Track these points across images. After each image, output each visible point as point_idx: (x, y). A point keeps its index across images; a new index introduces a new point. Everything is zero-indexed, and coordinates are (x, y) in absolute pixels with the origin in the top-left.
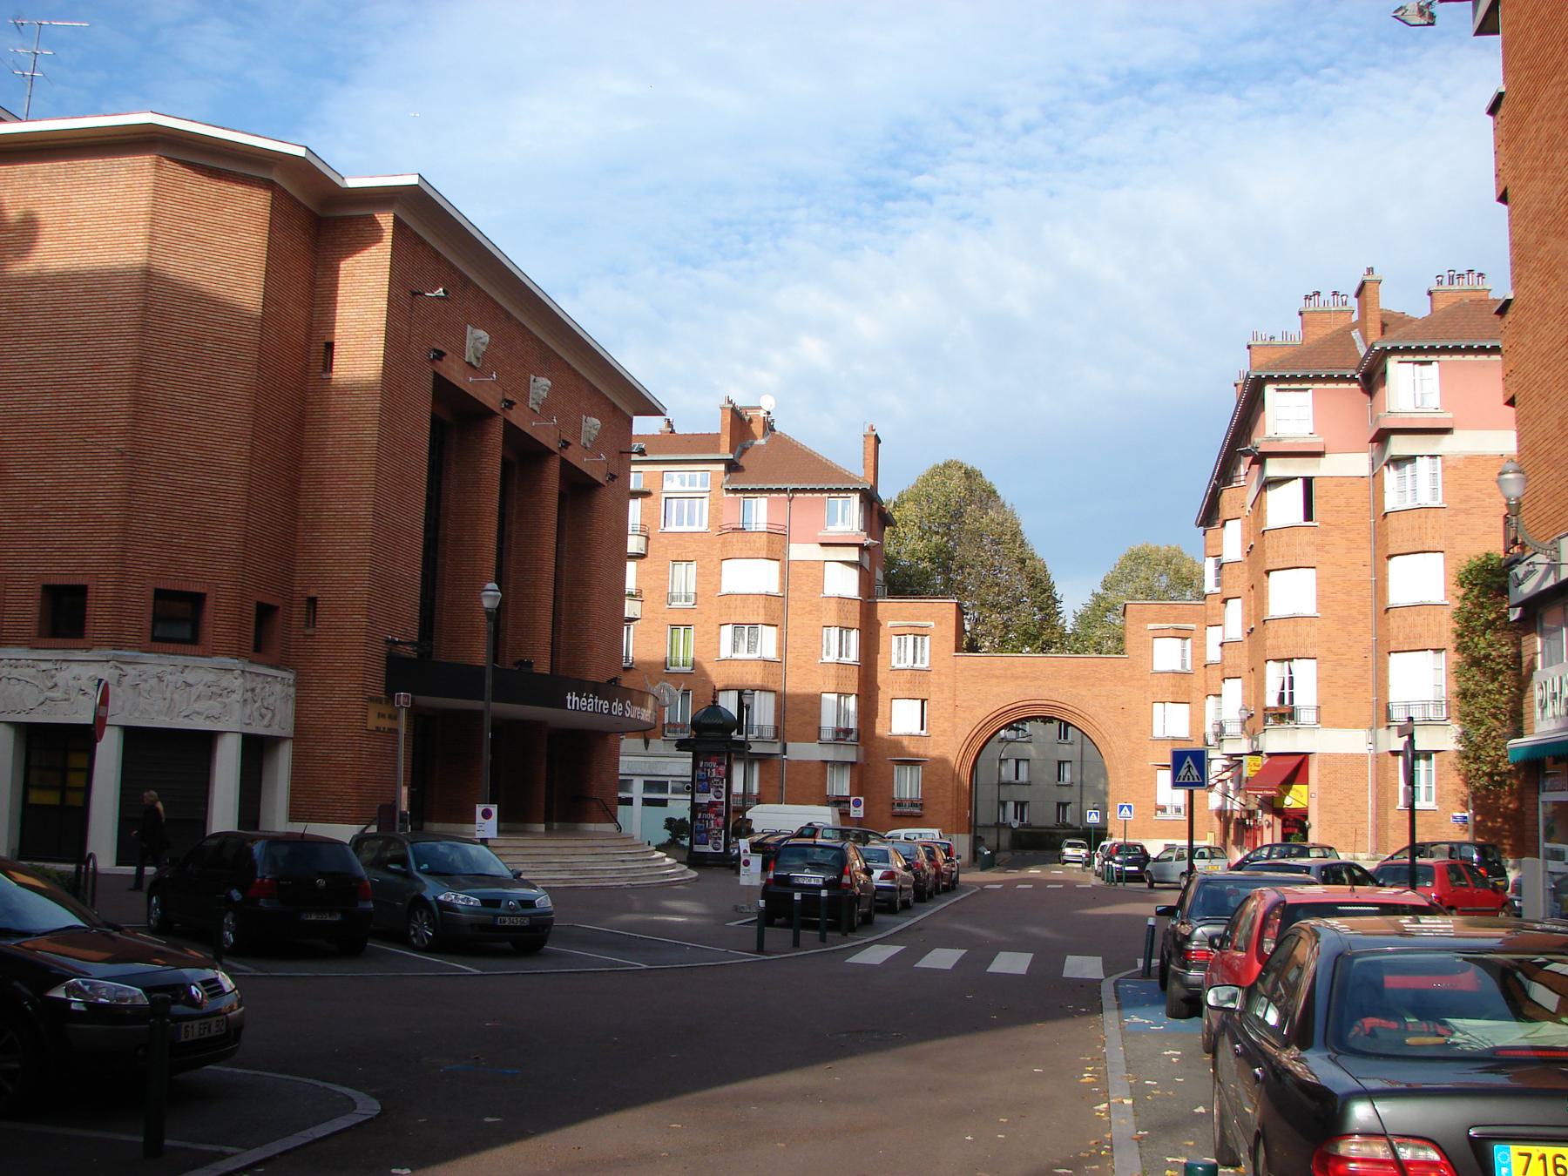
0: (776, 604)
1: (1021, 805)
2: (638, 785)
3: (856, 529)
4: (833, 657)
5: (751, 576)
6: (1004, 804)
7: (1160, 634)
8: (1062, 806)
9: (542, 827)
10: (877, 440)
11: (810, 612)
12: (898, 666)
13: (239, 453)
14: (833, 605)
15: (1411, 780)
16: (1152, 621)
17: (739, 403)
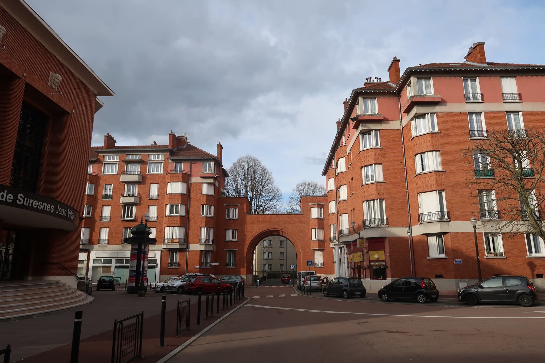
1: (270, 265)
3: (213, 172)
4: (205, 214)
6: (265, 265)
8: (282, 265)
9: (382, 267)
11: (197, 200)
14: (205, 197)
16: (310, 202)
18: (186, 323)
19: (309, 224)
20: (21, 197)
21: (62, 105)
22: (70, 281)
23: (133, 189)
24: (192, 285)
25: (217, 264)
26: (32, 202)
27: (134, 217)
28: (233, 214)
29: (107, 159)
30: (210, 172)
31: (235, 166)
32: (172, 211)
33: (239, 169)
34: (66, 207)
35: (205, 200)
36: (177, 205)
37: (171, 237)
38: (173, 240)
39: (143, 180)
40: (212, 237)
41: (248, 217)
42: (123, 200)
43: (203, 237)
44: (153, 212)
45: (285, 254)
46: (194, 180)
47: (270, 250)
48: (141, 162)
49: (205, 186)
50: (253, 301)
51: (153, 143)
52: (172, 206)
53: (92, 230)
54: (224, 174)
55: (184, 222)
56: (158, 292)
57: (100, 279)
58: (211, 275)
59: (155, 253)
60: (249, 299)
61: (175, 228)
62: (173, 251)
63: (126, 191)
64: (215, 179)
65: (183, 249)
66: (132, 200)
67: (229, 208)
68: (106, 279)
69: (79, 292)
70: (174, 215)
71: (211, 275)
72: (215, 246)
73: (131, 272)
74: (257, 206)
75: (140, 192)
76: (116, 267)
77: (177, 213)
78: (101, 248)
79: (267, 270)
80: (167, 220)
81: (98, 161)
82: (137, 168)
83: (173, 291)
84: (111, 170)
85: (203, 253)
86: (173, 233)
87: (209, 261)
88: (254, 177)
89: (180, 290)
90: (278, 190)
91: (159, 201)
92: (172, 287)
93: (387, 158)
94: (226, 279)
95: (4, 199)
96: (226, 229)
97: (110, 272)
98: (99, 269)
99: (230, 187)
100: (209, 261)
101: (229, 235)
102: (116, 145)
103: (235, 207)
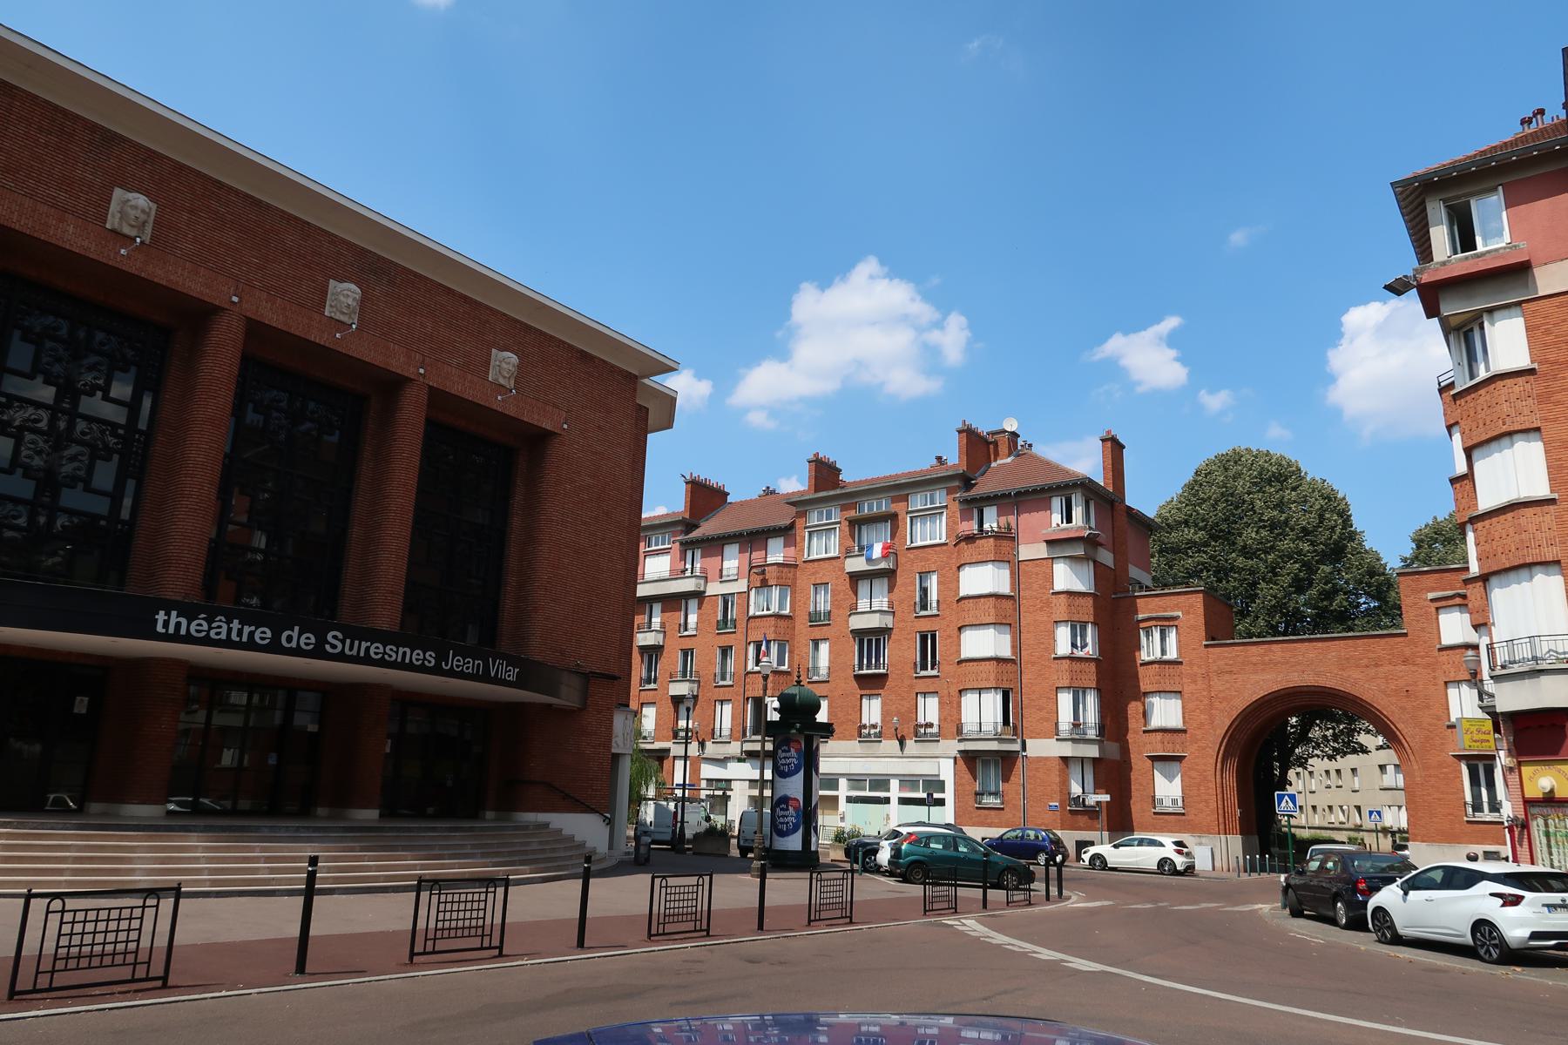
0: (1008, 604)
2: (843, 790)
3: (1080, 524)
5: (982, 579)
7: (1443, 604)
11: (1041, 609)
12: (1147, 659)
15: (1163, 639)
16: (1433, 590)
20: (335, 637)
26: (368, 649)
42: (857, 622)
51: (935, 462)
76: (850, 800)
93: (1558, 403)
95: (294, 644)
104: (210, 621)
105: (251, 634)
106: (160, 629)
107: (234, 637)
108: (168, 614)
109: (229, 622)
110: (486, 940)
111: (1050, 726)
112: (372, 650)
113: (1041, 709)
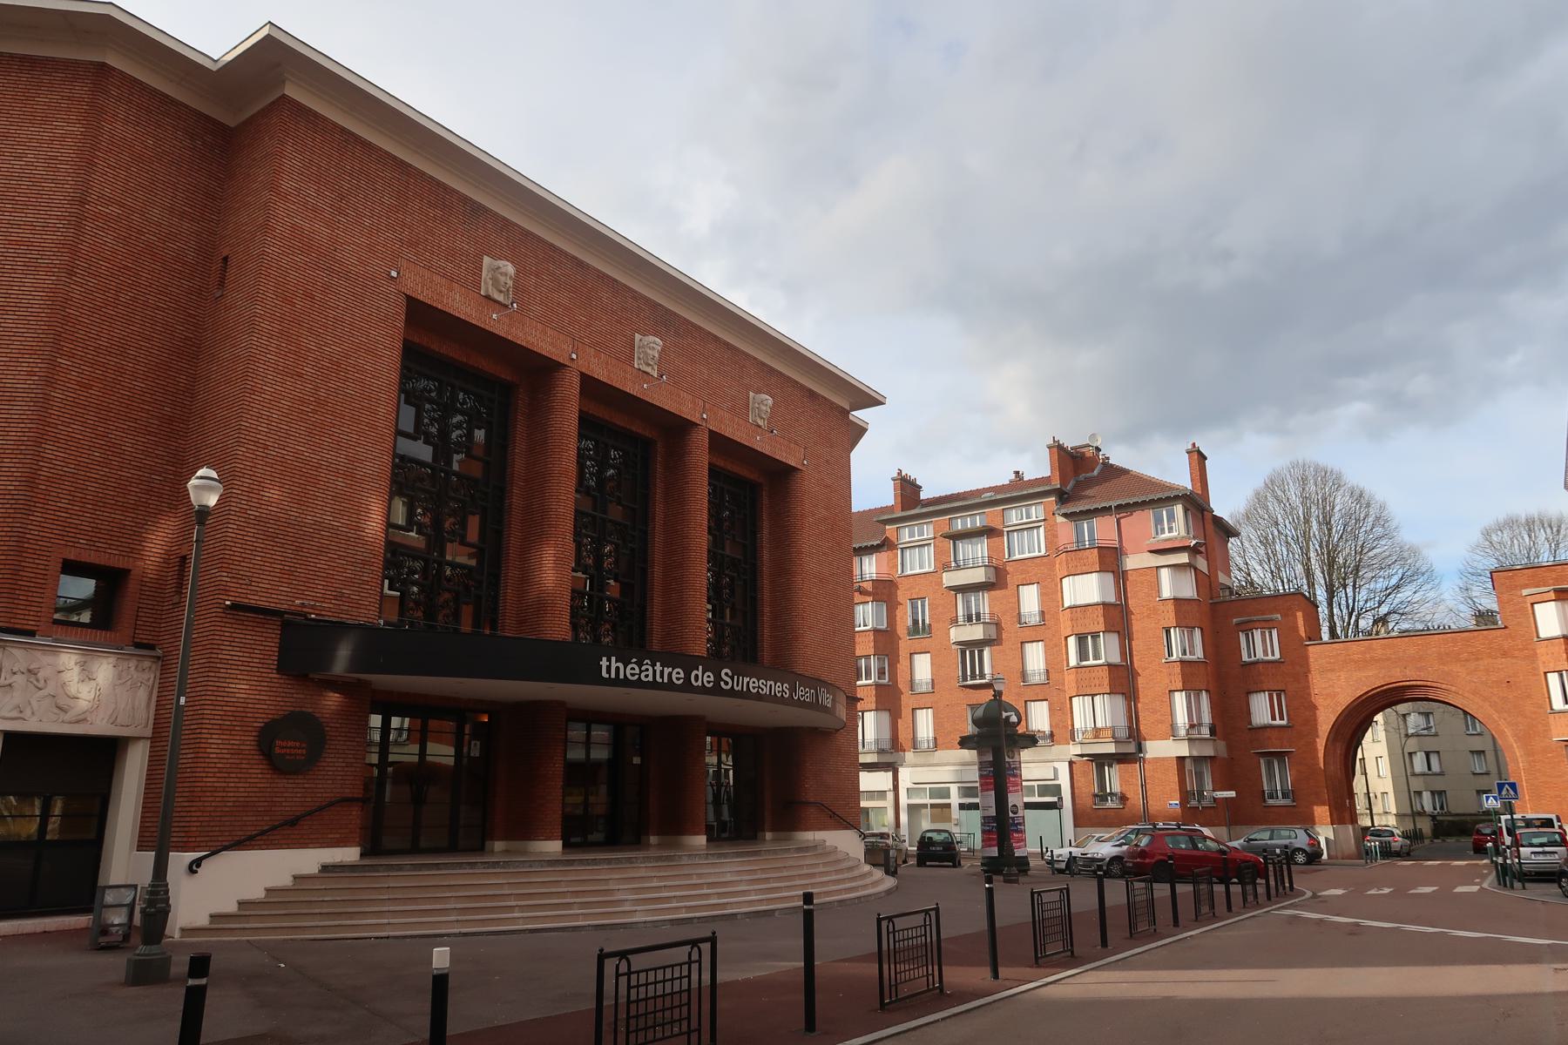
1: (1438, 794)
3: (1183, 533)
6: (1419, 793)
10: (1203, 458)
11: (1148, 616)
13: (31, 373)
14: (1171, 607)
16: (1526, 586)
17: (1069, 443)
18: (1056, 940)
19: (1533, 657)
21: (782, 455)
22: (847, 843)
23: (977, 605)
24: (1143, 854)
25: (1232, 794)
27: (988, 677)
28: (1262, 646)
29: (905, 536)
30: (1175, 534)
31: (1260, 500)
32: (1083, 655)
33: (1272, 505)
34: (815, 682)
35: (1172, 615)
36: (1095, 636)
37: (1090, 725)
38: (1097, 732)
39: (998, 580)
40: (1207, 718)
41: (1314, 651)
42: (956, 634)
43: (1181, 718)
44: (1036, 658)
45: (1490, 756)
46: (1132, 562)
47: (1431, 744)
48: (989, 532)
49: (1165, 574)
50: (1317, 902)
51: (1013, 477)
52: (1081, 639)
53: (895, 716)
54: (1225, 531)
55: (1123, 681)
56: (1061, 871)
57: (923, 838)
58: (1197, 827)
59: (1039, 768)
60: (1309, 894)
61: (1097, 698)
62: (1101, 761)
63: (960, 613)
64: (1194, 551)
65: (1129, 754)
66: (976, 632)
67: (1247, 628)
68: (937, 837)
69: (867, 868)
70: (1092, 662)
71: (1197, 827)
72: (1222, 745)
73: (986, 820)
74: (1350, 615)
75: (995, 610)
77: (1096, 657)
78: (921, 759)
79: (1428, 807)
80: (1073, 677)
81: (886, 545)
82: (978, 550)
83: (1100, 871)
84: (919, 562)
85: (1189, 765)
86: (1095, 714)
87: (1208, 784)
88: (1326, 522)
89: (1116, 869)
90: (1415, 551)
91: (1045, 629)
92: (1093, 860)
94: (1262, 836)
96: (1249, 693)
97: (949, 819)
98: (923, 811)
99: (1250, 564)
100: (1208, 784)
101: (1261, 710)
102: (923, 496)
103: (1268, 625)
104: (640, 664)
105: (670, 674)
106: (605, 675)
107: (659, 679)
108: (609, 660)
109: (653, 665)
110: (623, 968)
111: (1165, 728)
112: (674, 676)
113: (1155, 712)
